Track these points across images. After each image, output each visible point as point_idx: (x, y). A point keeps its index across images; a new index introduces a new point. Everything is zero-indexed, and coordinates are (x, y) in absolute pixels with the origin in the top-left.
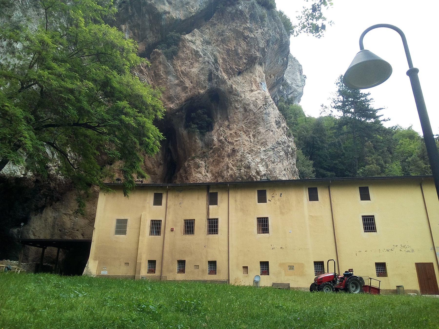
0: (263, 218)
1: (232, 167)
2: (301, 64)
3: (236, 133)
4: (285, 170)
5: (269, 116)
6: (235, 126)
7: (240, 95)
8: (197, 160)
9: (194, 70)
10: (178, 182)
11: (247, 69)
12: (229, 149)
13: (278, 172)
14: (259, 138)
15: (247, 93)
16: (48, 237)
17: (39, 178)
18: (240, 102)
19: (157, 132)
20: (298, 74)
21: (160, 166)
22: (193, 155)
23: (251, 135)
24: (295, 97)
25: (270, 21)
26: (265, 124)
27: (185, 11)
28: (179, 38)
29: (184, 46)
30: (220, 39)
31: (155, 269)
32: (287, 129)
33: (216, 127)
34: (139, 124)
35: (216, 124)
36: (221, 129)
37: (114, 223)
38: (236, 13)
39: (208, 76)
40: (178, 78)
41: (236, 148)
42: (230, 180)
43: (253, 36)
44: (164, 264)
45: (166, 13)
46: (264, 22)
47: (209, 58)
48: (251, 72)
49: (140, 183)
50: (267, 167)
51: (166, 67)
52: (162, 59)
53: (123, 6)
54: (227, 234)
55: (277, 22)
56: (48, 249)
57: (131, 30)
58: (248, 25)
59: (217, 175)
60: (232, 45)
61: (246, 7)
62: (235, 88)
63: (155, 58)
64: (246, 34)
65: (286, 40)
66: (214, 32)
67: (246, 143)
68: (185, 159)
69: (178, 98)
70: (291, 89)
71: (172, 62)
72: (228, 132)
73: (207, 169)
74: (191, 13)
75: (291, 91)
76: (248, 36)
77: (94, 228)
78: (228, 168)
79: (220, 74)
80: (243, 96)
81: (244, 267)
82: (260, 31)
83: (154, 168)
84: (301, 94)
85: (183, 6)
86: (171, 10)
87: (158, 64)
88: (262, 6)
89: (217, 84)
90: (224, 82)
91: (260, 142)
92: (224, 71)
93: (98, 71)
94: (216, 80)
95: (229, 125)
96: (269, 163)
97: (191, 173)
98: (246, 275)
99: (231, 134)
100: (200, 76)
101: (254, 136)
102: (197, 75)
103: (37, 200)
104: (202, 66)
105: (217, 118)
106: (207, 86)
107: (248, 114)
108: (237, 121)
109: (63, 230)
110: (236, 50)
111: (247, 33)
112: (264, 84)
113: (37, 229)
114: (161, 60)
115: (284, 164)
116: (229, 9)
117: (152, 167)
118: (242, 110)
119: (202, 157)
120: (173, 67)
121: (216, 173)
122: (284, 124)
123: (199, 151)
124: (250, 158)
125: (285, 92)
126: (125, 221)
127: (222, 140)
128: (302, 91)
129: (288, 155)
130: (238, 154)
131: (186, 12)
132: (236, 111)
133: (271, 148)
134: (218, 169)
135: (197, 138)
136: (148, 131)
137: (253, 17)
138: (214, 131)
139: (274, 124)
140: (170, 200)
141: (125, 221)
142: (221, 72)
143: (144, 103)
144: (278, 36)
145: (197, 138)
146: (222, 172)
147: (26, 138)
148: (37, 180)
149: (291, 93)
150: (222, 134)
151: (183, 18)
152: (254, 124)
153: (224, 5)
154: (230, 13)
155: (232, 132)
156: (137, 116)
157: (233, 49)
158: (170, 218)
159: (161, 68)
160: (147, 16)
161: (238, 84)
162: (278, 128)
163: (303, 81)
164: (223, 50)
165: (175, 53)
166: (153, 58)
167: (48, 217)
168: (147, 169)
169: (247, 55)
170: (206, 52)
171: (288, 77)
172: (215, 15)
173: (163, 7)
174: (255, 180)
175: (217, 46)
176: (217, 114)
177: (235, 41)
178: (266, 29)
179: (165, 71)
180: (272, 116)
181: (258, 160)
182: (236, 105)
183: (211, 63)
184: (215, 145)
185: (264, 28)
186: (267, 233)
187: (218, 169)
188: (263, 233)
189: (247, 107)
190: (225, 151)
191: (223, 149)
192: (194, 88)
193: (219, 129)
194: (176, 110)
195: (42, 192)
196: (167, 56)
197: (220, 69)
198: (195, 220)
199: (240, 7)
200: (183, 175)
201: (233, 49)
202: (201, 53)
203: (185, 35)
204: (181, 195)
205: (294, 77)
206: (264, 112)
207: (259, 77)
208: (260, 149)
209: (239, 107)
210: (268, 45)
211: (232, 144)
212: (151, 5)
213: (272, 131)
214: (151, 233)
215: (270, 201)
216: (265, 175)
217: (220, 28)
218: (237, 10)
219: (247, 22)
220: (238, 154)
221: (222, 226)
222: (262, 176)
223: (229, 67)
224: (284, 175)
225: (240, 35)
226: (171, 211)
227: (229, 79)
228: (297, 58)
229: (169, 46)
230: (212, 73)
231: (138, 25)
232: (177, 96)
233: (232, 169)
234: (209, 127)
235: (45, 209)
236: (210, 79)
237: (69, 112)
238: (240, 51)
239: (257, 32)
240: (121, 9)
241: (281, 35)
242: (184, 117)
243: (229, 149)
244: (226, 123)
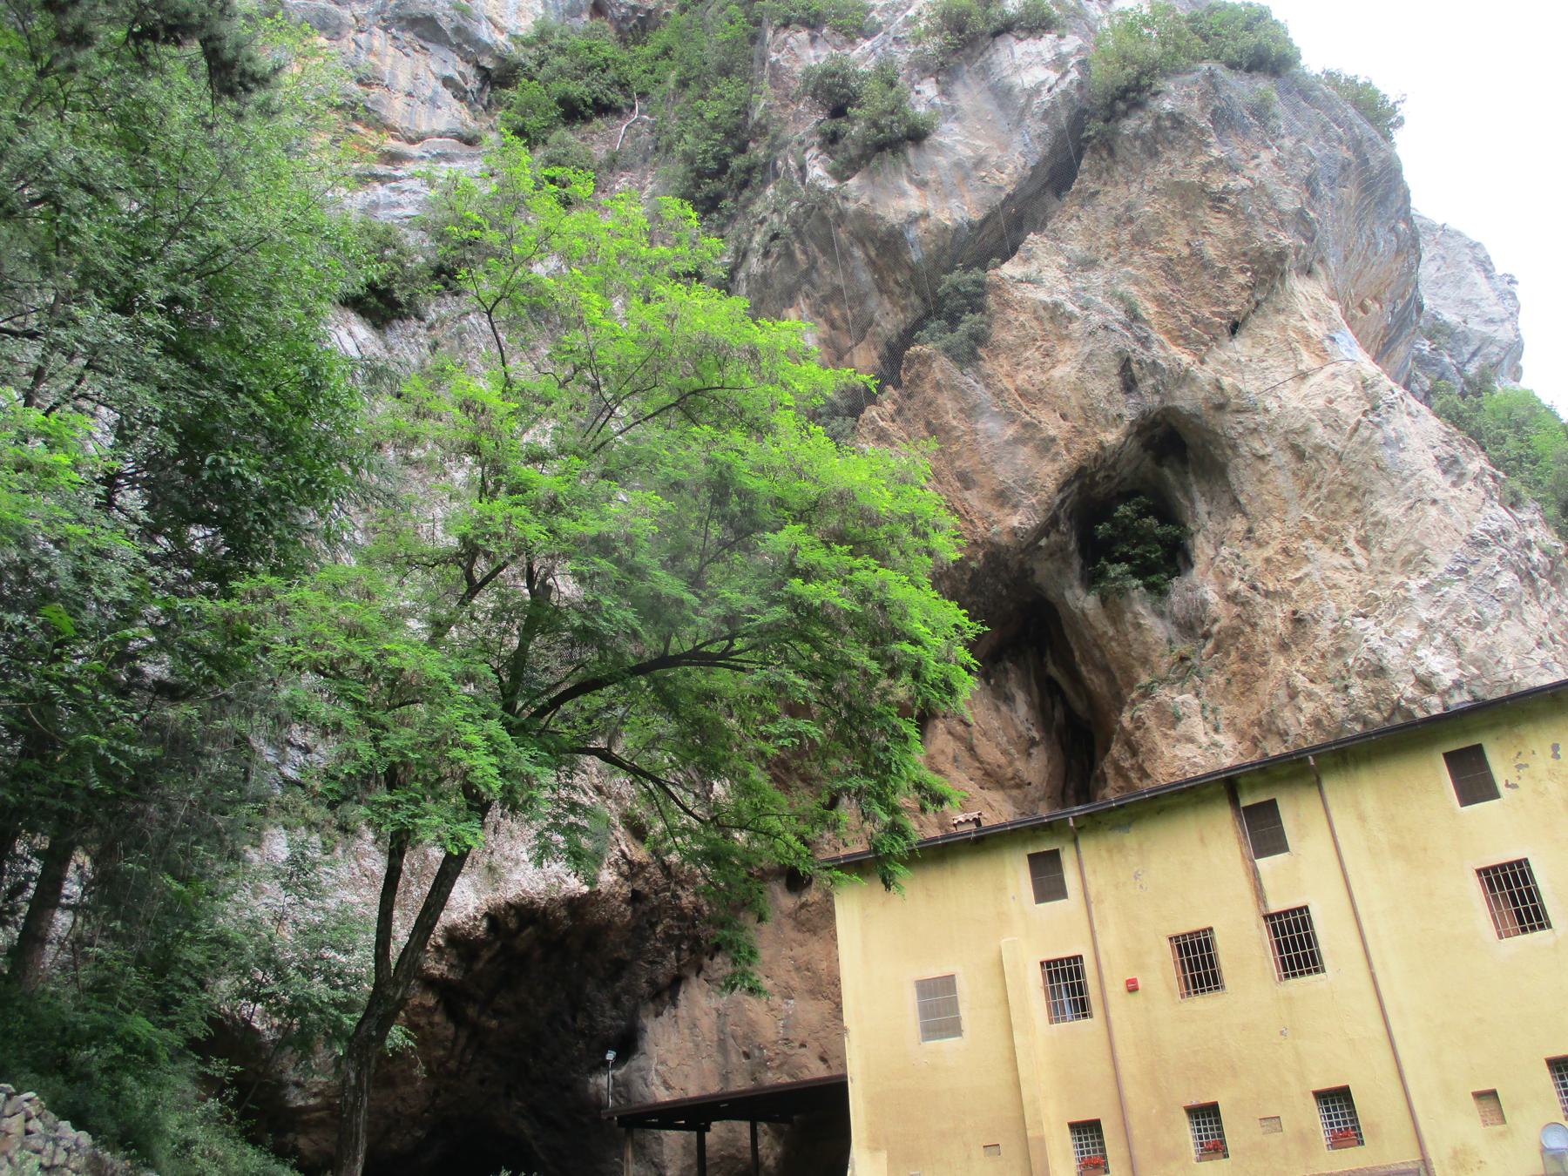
0: (1502, 867)
1: (1311, 686)
2: (1476, 240)
3: (1285, 551)
4: (1540, 644)
5: (1402, 450)
6: (1276, 525)
7: (1260, 405)
8: (1163, 694)
9: (1057, 373)
10: (1111, 794)
11: (1258, 304)
12: (1275, 619)
13: (1510, 660)
14: (1388, 544)
15: (1286, 392)
16: (714, 1087)
17: (640, 884)
18: (1270, 429)
19: (953, 613)
20: (1478, 277)
21: (1034, 751)
22: (1145, 679)
23: (1351, 544)
24: (1494, 366)
25: (1296, 111)
26: (1397, 482)
27: (976, 190)
28: (979, 283)
29: (1006, 304)
30: (1125, 237)
31: (1105, 1157)
32: (1494, 477)
33: (1202, 549)
34: (864, 596)
35: (1200, 540)
36: (1224, 551)
37: (911, 998)
38: (1158, 128)
39: (1119, 374)
40: (1011, 418)
41: (1306, 608)
42: (1314, 738)
43: (1244, 183)
44: (1137, 1132)
45: (914, 219)
46: (1272, 123)
47: (1102, 311)
48: (1278, 311)
49: (973, 827)
50: (1459, 651)
51: (960, 393)
52: (942, 371)
53: (775, 250)
54: (1363, 964)
55: (1326, 104)
56: (718, 1131)
57: (819, 314)
58: (1215, 152)
59: (1256, 731)
60: (1177, 242)
61: (1189, 97)
62: (1234, 386)
63: (918, 376)
64: (1216, 187)
65: (1382, 155)
66: (1097, 219)
67: (1341, 579)
68: (1119, 702)
69: (1030, 488)
70: (1467, 340)
71: (978, 371)
72: (1255, 557)
73: (1211, 717)
74: (1000, 188)
75: (1471, 349)
76: (1227, 191)
77: (845, 1030)
78: (1293, 694)
79: (1162, 353)
80: (1272, 404)
81: (1478, 1096)
82: (1265, 157)
83: (1011, 763)
84: (1515, 349)
85: (966, 177)
86: (930, 205)
87: (930, 393)
88: (1249, 70)
89: (1158, 392)
90: (1185, 378)
91: (1398, 559)
92: (1174, 340)
93: (691, 450)
94: (1151, 381)
95: (1250, 531)
96: (1459, 633)
97: (1152, 751)
98: (1500, 1128)
99: (1268, 561)
100: (1090, 386)
101: (1364, 542)
102: (1078, 386)
103: (652, 963)
104: (1087, 349)
105: (1195, 515)
106: (1126, 412)
107: (1313, 465)
108: (1275, 504)
109: (757, 1052)
110: (1197, 255)
111: (1218, 182)
112: (1346, 337)
113: (672, 1064)
114: (939, 376)
115: (1532, 621)
116: (1129, 125)
117: (1003, 760)
118: (1284, 458)
119: (1179, 679)
120: (987, 386)
121: (1252, 724)
122: (1476, 463)
123: (1162, 656)
124: (1371, 631)
125: (1447, 359)
126: (948, 983)
127: (1237, 593)
128: (1518, 336)
129: (1533, 581)
130: (1318, 630)
131: (982, 194)
132: (1264, 469)
133: (1451, 571)
134: (1255, 707)
135: (1141, 607)
136: (904, 615)
137: (1223, 119)
138: (1199, 566)
139: (1435, 474)
140: (1091, 866)
141: (948, 983)
142: (1162, 347)
143: (872, 519)
144: (1344, 153)
145: (1141, 607)
146: (1271, 714)
147: (468, 747)
148: (634, 891)
149: (1474, 354)
150: (1232, 571)
151: (977, 216)
152: (1349, 495)
153: (1107, 120)
154: (1137, 136)
155: (1268, 552)
156: (851, 571)
157: (1186, 252)
158: (1109, 940)
159: (946, 402)
160: (858, 252)
161: (1239, 367)
162: (1454, 484)
163: (1507, 290)
164: (1149, 268)
165: (978, 338)
166: (911, 381)
167: (697, 1013)
168: (987, 774)
169: (1245, 254)
170: (1088, 295)
171: (1439, 302)
172: (1084, 164)
173: (901, 204)
174: (1420, 714)
175: (1123, 261)
176: (1192, 501)
177: (1183, 223)
178: (1288, 143)
179: (961, 410)
180: (1414, 442)
181: (1410, 631)
182: (1257, 445)
183: (1117, 326)
184: (1215, 620)
185: (1278, 142)
186: (1542, 927)
187: (1255, 707)
188: (1524, 930)
189: (1300, 441)
190: (1264, 632)
191: (1254, 626)
192: (1080, 433)
193: (1218, 554)
194: (1035, 529)
195: (659, 929)
196: (955, 358)
197: (1154, 336)
198: (1211, 929)
199: (1167, 105)
200: (1127, 765)
201: (1186, 252)
202: (1069, 307)
203: (996, 267)
204: (1131, 839)
205: (1463, 293)
206: (1378, 436)
207: (1316, 317)
208: (1402, 585)
209: (1269, 450)
210: (1313, 194)
211: (1284, 595)
212: (860, 215)
213: (1434, 502)
214: (1056, 1014)
215: (1514, 786)
216: (1458, 685)
217: (1118, 200)
218: (1158, 118)
219: (1208, 145)
220: (1318, 630)
221: (1329, 932)
222: (1447, 692)
223: (1186, 319)
224: (1543, 665)
225: (1192, 197)
226: (1107, 911)
227: (1202, 362)
228: (1453, 225)
229: (953, 321)
230: (1128, 359)
231: (837, 291)
232: (1024, 480)
233: (1310, 696)
234: (1176, 557)
235: (682, 989)
236: (1129, 384)
237: (606, 620)
238: (1210, 252)
239: (1258, 166)
240: (770, 261)
241: (1357, 145)
242: (1072, 546)
243: (1275, 619)
244: (1239, 524)
